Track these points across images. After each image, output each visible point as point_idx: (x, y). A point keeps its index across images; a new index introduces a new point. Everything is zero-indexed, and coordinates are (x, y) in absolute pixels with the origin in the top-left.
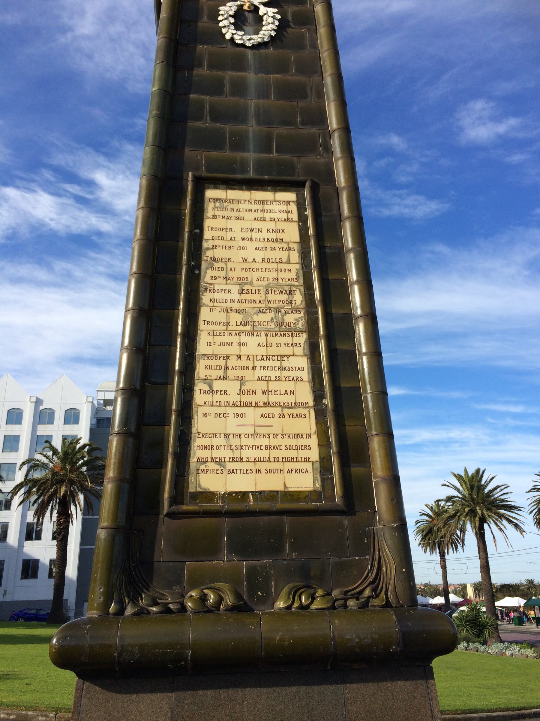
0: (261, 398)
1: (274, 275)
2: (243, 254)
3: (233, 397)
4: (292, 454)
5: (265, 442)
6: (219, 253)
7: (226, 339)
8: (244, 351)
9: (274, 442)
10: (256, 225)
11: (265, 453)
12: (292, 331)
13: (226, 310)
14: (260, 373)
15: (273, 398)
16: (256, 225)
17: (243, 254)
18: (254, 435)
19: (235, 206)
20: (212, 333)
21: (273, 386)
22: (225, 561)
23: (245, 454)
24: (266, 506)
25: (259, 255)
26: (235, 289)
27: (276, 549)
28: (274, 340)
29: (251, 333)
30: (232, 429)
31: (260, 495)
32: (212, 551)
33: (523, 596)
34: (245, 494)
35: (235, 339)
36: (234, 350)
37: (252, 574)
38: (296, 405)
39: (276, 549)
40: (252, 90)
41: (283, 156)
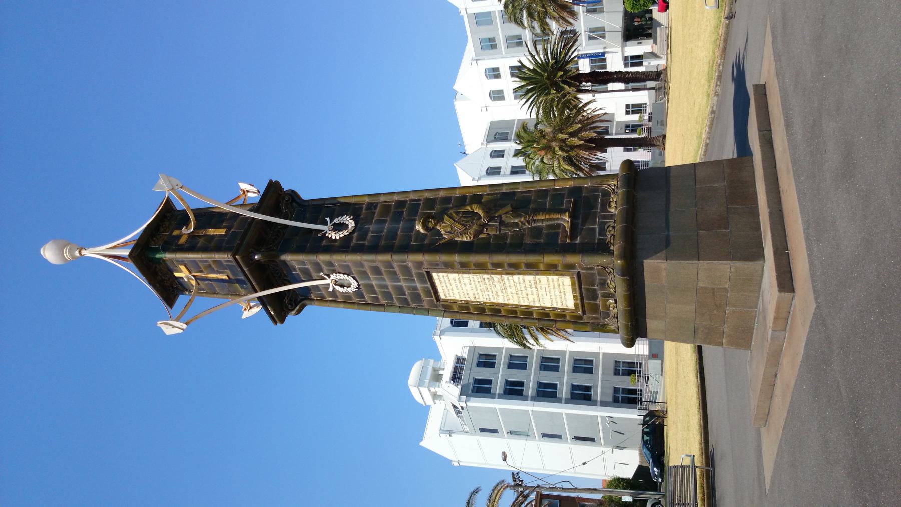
0: (534, 290)
5: (552, 290)
8: (514, 292)
11: (557, 290)
14: (523, 288)
15: (533, 286)
22: (599, 302)
24: (577, 289)
30: (548, 297)
31: (574, 290)
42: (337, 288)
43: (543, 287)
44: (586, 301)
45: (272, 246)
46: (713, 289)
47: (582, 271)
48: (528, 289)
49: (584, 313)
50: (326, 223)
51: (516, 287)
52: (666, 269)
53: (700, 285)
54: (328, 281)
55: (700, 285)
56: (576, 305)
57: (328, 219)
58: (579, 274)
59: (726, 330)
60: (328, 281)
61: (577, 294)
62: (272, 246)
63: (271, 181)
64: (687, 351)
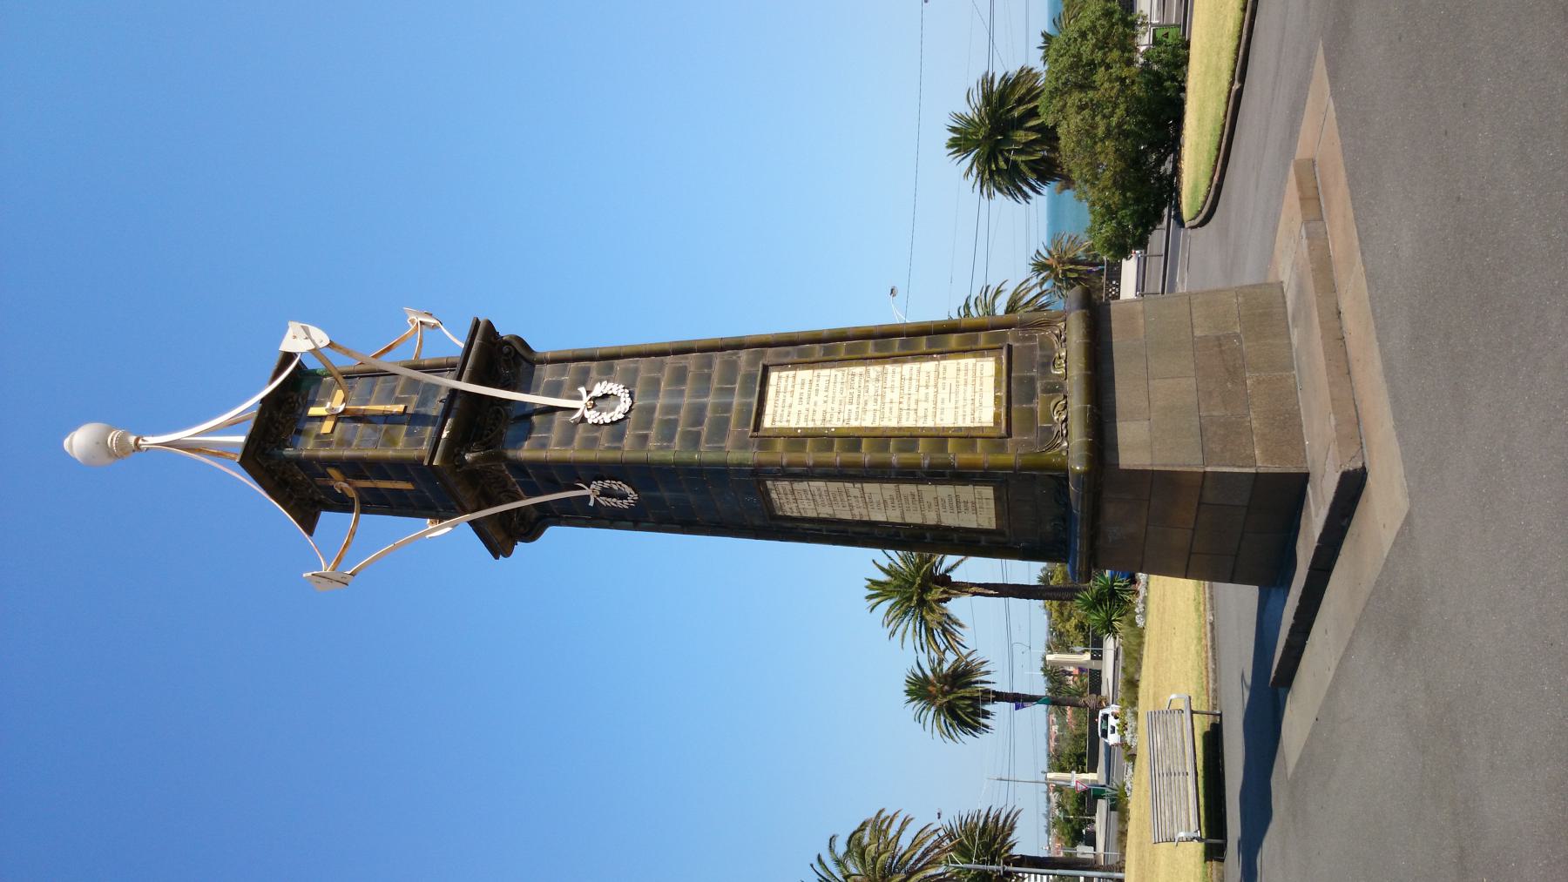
0: (931, 390)
1: (839, 386)
2: (820, 403)
3: (930, 405)
4: (970, 373)
5: (962, 388)
6: (819, 417)
7: (887, 410)
8: (896, 399)
9: (962, 382)
10: (797, 395)
11: (970, 388)
12: (884, 373)
13: (865, 411)
14: (913, 390)
15: (932, 383)
16: (797, 395)
17: (820, 403)
18: (957, 393)
19: (779, 410)
20: (882, 418)
21: (923, 383)
22: (1038, 405)
23: (969, 397)
24: (1004, 385)
25: (822, 393)
26: (848, 407)
27: (1032, 380)
28: (889, 384)
29: (883, 396)
30: (953, 405)
31: (997, 387)
32: (1032, 412)
33: (519, 467)
34: (996, 397)
35: (887, 406)
36: (895, 407)
37: (1045, 391)
38: (937, 371)
39: (1032, 380)
40: (675, 401)
41: (739, 380)
42: (602, 500)
43: (948, 382)
44: (1015, 406)
45: (485, 453)
46: (1218, 338)
47: (1015, 345)
48: (923, 390)
49: (1009, 434)
50: (579, 398)
51: (902, 388)
52: (1144, 311)
53: (1198, 333)
54: (587, 492)
55: (1198, 333)
56: (997, 417)
57: (582, 390)
58: (1010, 348)
59: (1255, 424)
60: (587, 492)
61: (1003, 393)
62: (485, 453)
63: (961, 142)
64: (1137, 446)
